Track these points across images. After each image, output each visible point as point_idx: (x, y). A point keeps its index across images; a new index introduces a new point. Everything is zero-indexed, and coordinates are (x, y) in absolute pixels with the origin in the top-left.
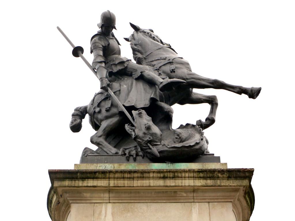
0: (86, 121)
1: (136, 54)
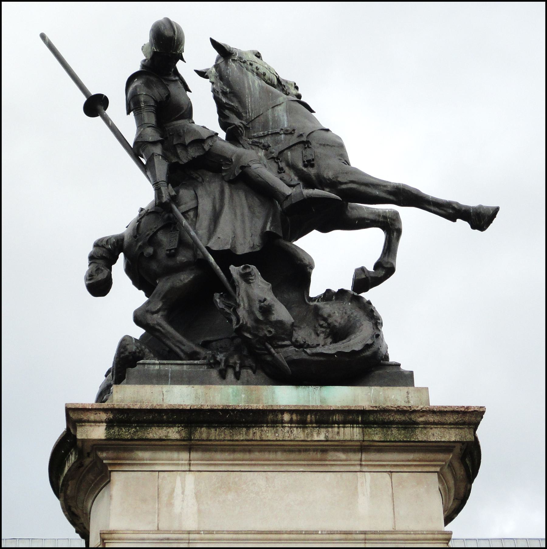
0: (119, 269)
1: (227, 117)
